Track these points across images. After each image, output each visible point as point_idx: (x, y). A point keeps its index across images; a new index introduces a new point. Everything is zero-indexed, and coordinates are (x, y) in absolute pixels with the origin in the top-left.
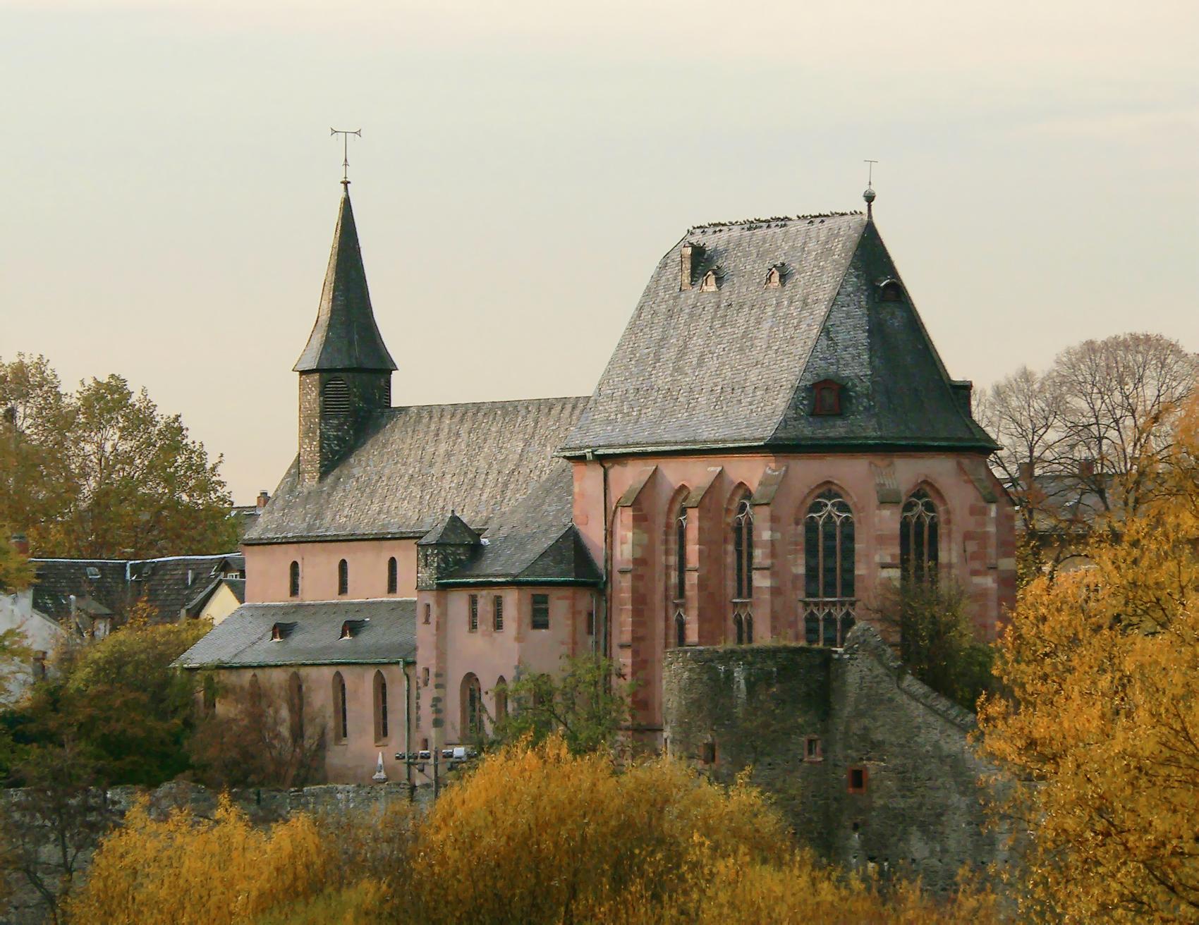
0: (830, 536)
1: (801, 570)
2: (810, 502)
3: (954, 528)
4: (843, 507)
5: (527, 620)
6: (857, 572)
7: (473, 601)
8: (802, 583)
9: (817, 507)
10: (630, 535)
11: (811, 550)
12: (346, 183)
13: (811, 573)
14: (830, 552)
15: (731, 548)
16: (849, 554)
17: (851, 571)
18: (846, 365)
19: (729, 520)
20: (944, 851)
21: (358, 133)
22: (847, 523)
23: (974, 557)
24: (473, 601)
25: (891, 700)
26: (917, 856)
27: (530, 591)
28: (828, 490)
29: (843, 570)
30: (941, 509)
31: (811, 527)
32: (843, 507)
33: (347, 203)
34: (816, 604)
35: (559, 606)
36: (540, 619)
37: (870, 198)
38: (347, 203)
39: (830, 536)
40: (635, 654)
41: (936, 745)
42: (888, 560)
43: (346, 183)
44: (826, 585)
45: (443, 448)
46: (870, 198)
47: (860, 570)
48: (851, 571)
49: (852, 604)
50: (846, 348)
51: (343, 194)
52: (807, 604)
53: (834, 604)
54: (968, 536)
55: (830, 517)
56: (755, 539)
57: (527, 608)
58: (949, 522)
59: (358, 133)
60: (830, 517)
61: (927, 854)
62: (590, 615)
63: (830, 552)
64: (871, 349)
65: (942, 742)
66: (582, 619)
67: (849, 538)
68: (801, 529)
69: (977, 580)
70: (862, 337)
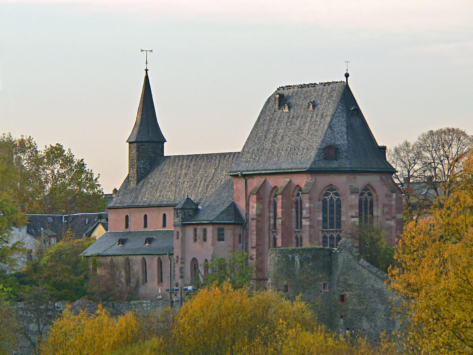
0: (332, 205)
1: (321, 218)
2: (324, 192)
3: (379, 202)
4: (337, 194)
5: (216, 237)
6: (342, 219)
7: (195, 230)
8: (321, 223)
9: (327, 194)
10: (255, 205)
11: (324, 211)
12: (147, 70)
13: (325, 220)
14: (332, 212)
15: (294, 210)
16: (339, 212)
17: (339, 218)
18: (338, 140)
19: (293, 199)
20: (376, 326)
21: (151, 51)
22: (338, 200)
23: (387, 213)
24: (195, 230)
25: (355, 268)
26: (365, 328)
27: (217, 226)
28: (331, 188)
29: (337, 219)
30: (374, 195)
31: (325, 202)
32: (337, 194)
33: (147, 78)
34: (327, 231)
35: (228, 232)
36: (221, 237)
37: (347, 75)
38: (147, 78)
39: (332, 205)
40: (257, 251)
41: (372, 286)
42: (354, 214)
43: (147, 70)
44: (330, 224)
45: (184, 172)
46: (347, 75)
47: (343, 218)
48: (340, 219)
49: (340, 231)
50: (338, 134)
51: (145, 74)
52: (323, 232)
53: (333, 231)
54: (384, 205)
55: (332, 198)
56: (303, 206)
57: (216, 233)
58: (377, 200)
59: (151, 51)
60: (332, 198)
61: (369, 327)
62: (240, 235)
63: (332, 212)
64: (348, 133)
65: (375, 285)
66: (237, 237)
67: (339, 206)
68: (321, 203)
69: (388, 222)
70: (344, 129)
